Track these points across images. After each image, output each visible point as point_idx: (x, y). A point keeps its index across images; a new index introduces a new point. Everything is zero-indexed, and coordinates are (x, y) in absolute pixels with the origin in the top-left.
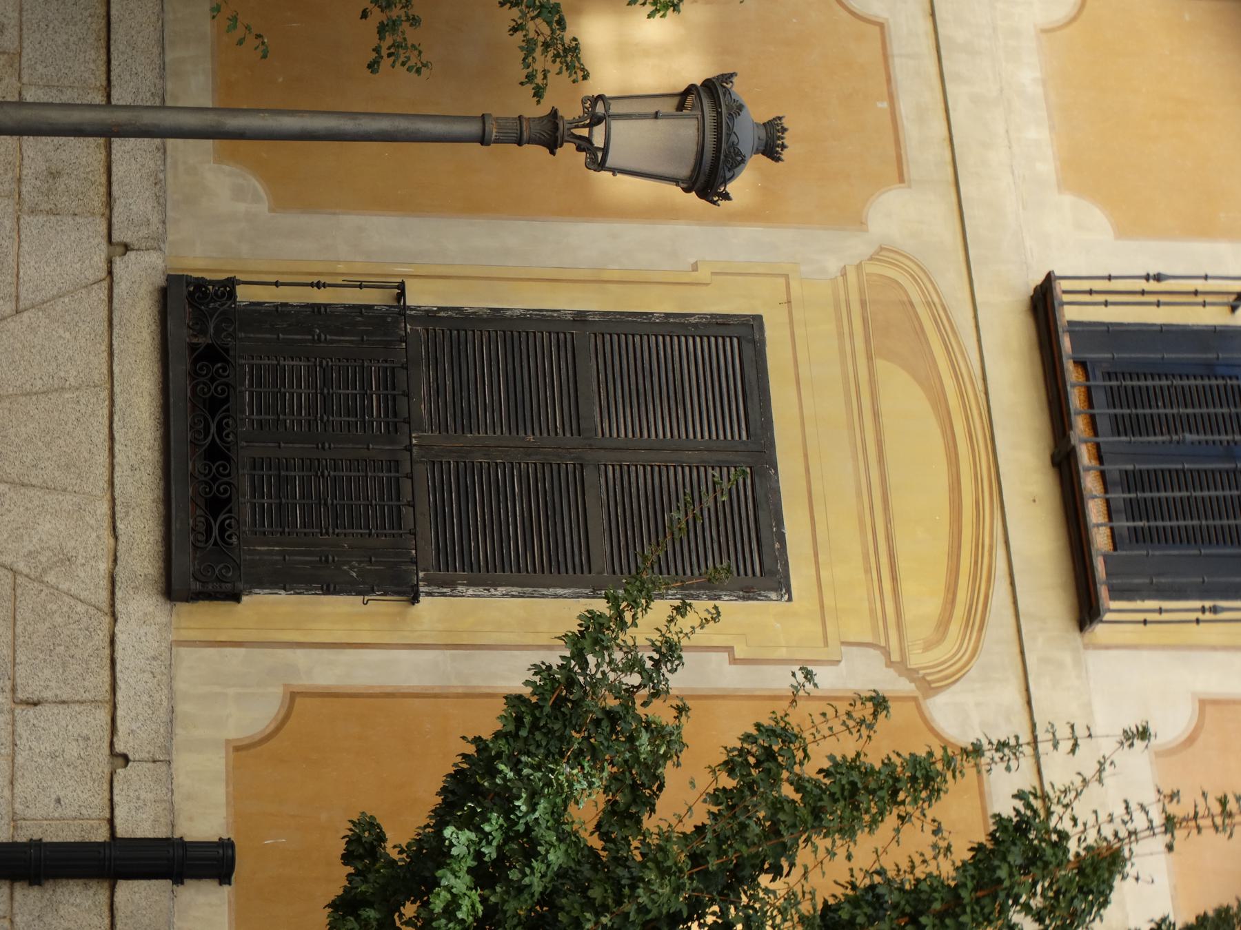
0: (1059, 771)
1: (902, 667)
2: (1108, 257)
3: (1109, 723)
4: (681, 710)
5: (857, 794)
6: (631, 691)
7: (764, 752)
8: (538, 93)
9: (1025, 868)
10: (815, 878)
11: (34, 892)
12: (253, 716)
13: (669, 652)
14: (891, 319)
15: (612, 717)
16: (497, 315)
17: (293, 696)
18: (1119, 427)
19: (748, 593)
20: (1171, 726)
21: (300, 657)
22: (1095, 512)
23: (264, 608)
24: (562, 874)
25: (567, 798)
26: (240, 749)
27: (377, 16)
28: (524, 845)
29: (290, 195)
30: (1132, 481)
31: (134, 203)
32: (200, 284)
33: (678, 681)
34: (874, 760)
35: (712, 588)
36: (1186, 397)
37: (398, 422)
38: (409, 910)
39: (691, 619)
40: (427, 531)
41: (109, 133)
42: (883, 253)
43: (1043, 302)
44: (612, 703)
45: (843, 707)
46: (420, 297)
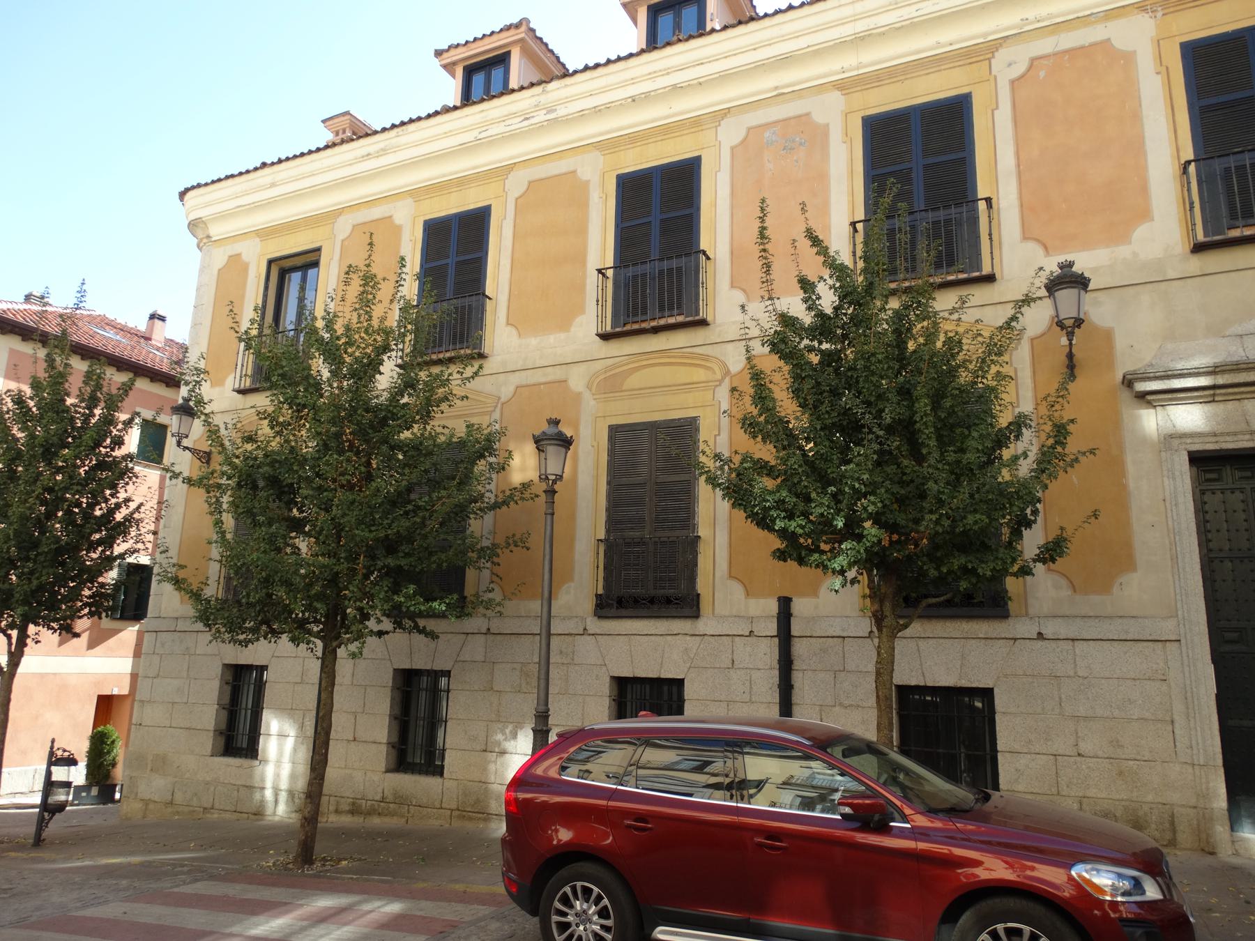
0: (755, 332)
1: (721, 381)
2: (590, 318)
3: (739, 317)
4: (736, 452)
5: (762, 396)
6: (730, 468)
7: (750, 425)
8: (537, 496)
9: (786, 344)
10: (789, 411)
11: (795, 662)
12: (737, 590)
13: (717, 457)
14: (610, 384)
15: (738, 475)
16: (607, 510)
17: (731, 577)
18: (644, 313)
19: (697, 430)
20: (739, 297)
21: (717, 575)
22: (672, 320)
23: (702, 586)
24: (790, 491)
25: (765, 491)
26: (748, 594)
27: (512, 547)
28: (780, 504)
29: (568, 576)
30: (662, 309)
31: (571, 627)
32: (597, 606)
33: (726, 454)
34: (752, 391)
35: (696, 442)
36: (635, 292)
37: (641, 542)
38: (802, 540)
39: (707, 449)
40: (678, 533)
41: (549, 635)
42: (589, 387)
43: (605, 337)
44: (734, 475)
45: (735, 401)
46: (602, 534)
